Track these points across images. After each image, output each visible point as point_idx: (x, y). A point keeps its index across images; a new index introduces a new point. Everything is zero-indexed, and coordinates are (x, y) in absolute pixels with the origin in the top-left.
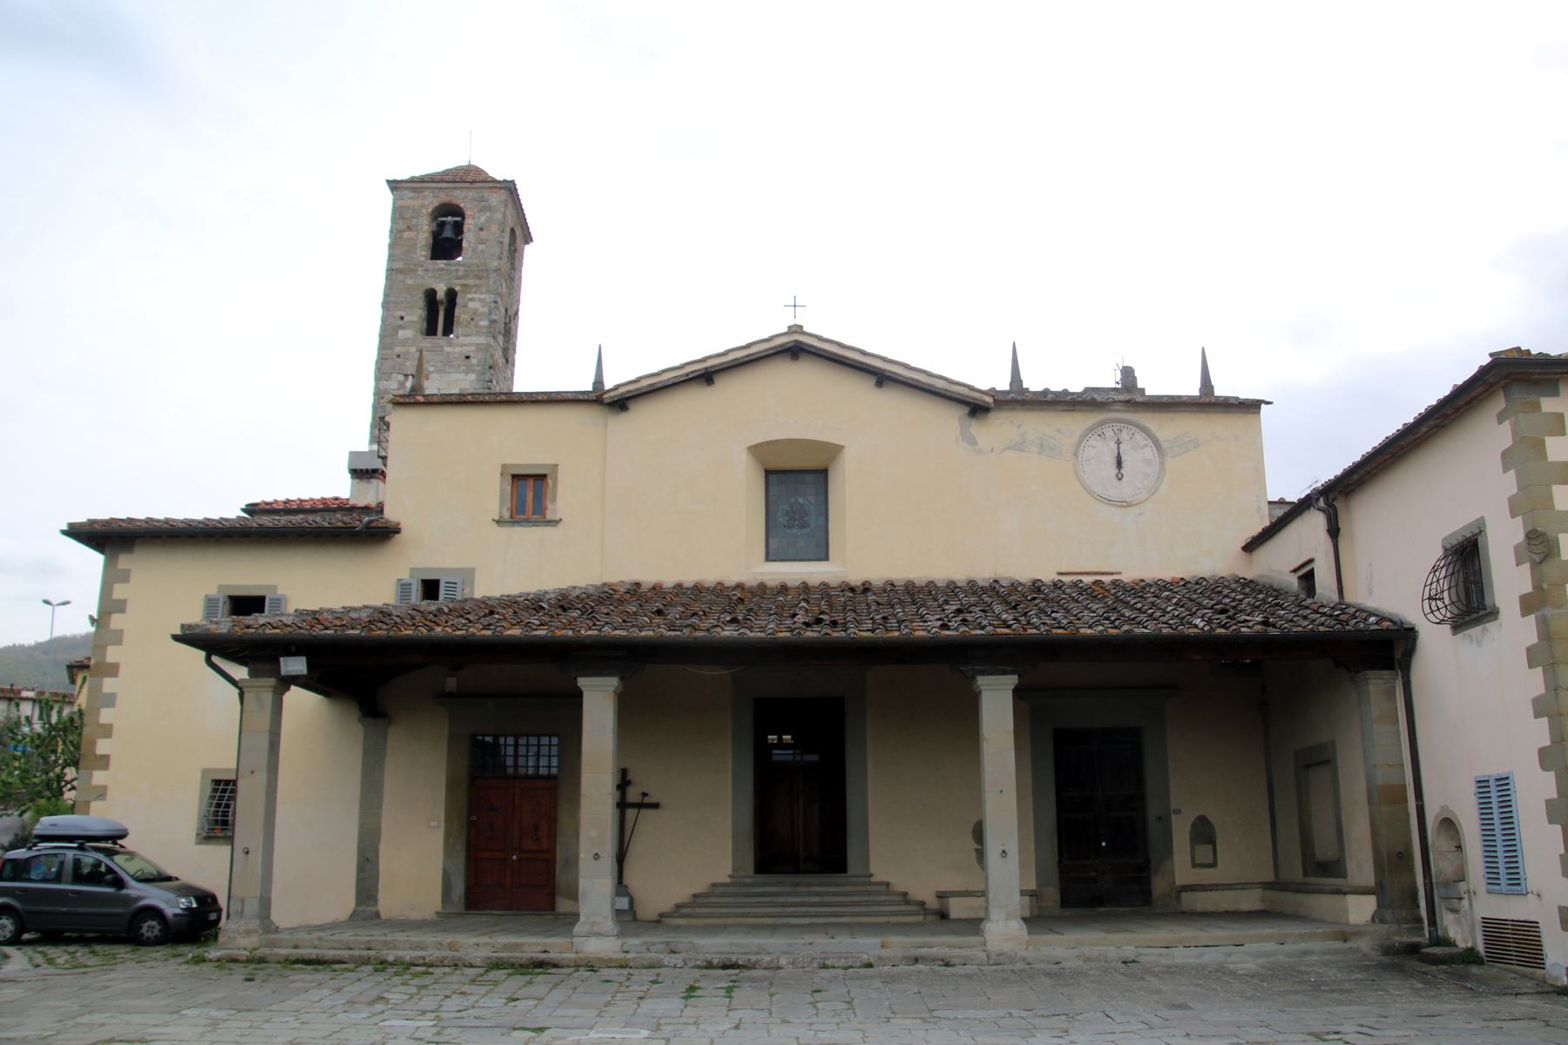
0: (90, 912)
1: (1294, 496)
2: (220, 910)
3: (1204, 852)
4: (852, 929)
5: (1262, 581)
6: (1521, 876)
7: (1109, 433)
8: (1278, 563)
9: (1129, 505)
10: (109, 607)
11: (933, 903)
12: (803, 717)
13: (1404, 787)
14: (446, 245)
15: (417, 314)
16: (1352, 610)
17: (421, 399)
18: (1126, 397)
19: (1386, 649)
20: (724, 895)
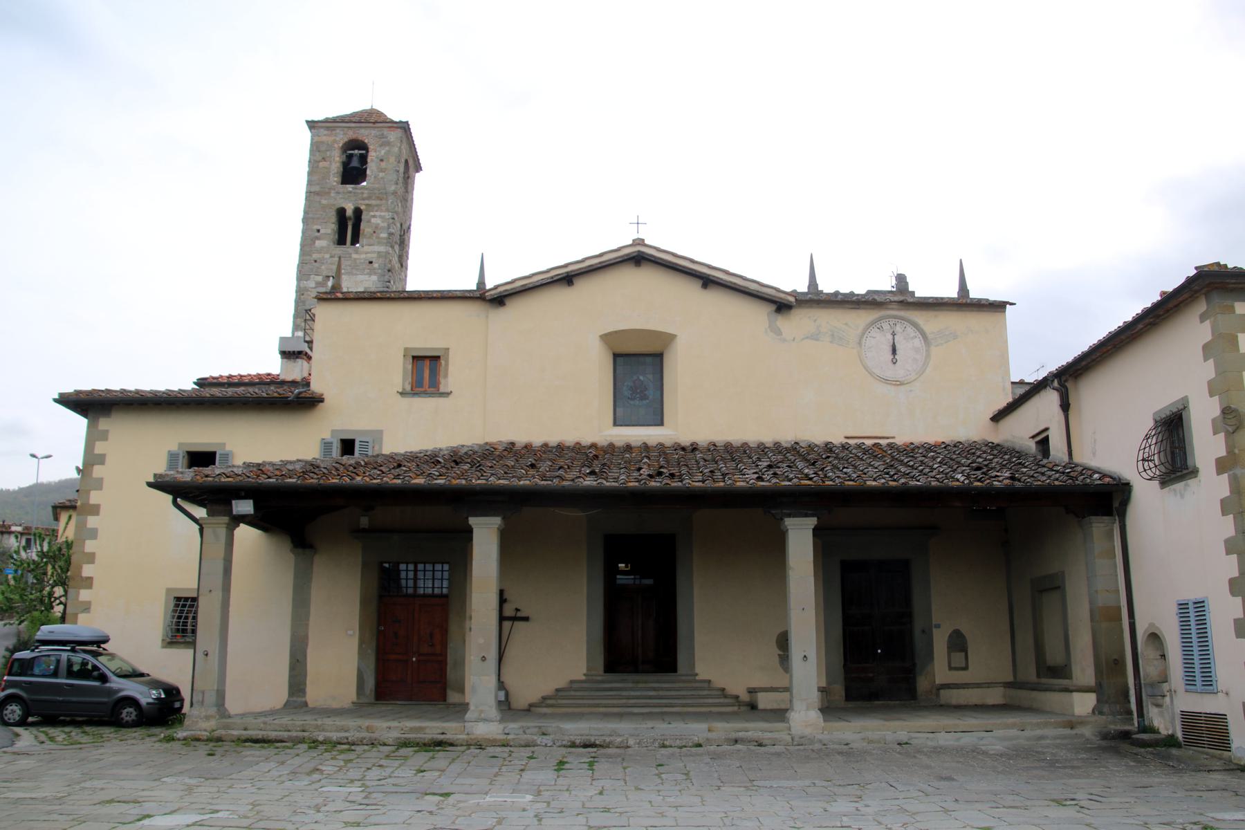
0: (79, 700)
1: (1031, 378)
2: (182, 700)
3: (958, 658)
4: (683, 716)
5: (1006, 445)
6: (1213, 678)
7: (886, 326)
8: (1019, 431)
9: (902, 384)
10: (92, 459)
11: (745, 697)
12: (643, 550)
13: (1119, 609)
14: (353, 173)
15: (330, 228)
16: (1080, 469)
17: (340, 295)
18: (901, 298)
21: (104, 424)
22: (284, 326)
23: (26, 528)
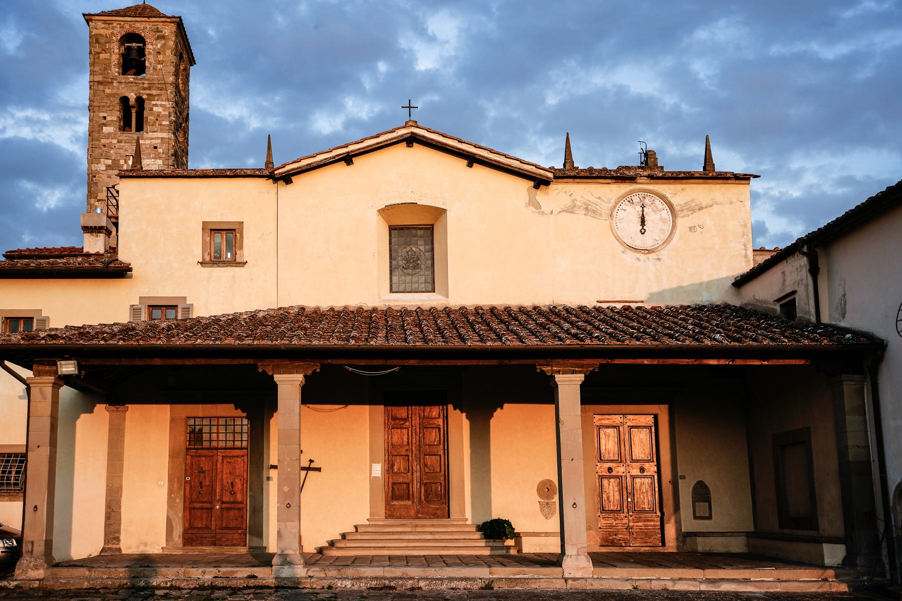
3: (702, 507)
7: (636, 199)
13: (868, 463)
14: (133, 63)
15: (114, 116)
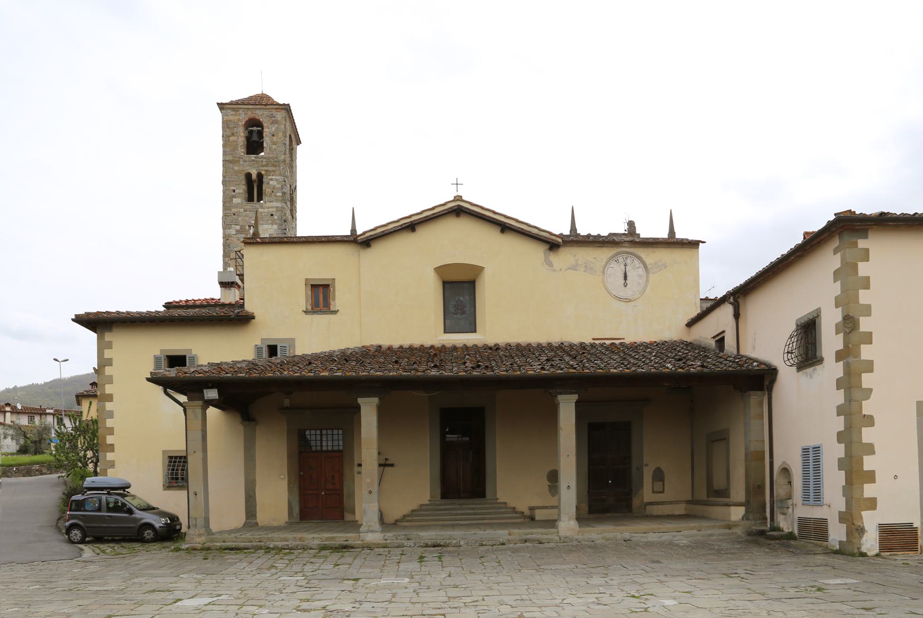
0: (105, 524)
2: (181, 524)
3: (658, 486)
4: (491, 526)
5: (695, 343)
7: (621, 260)
8: (705, 333)
9: (630, 301)
10: (103, 363)
11: (527, 513)
13: (764, 452)
14: (254, 145)
15: (242, 189)
16: (744, 359)
19: (761, 379)
20: (427, 510)
21: (108, 337)
22: (218, 264)
23: (56, 411)
